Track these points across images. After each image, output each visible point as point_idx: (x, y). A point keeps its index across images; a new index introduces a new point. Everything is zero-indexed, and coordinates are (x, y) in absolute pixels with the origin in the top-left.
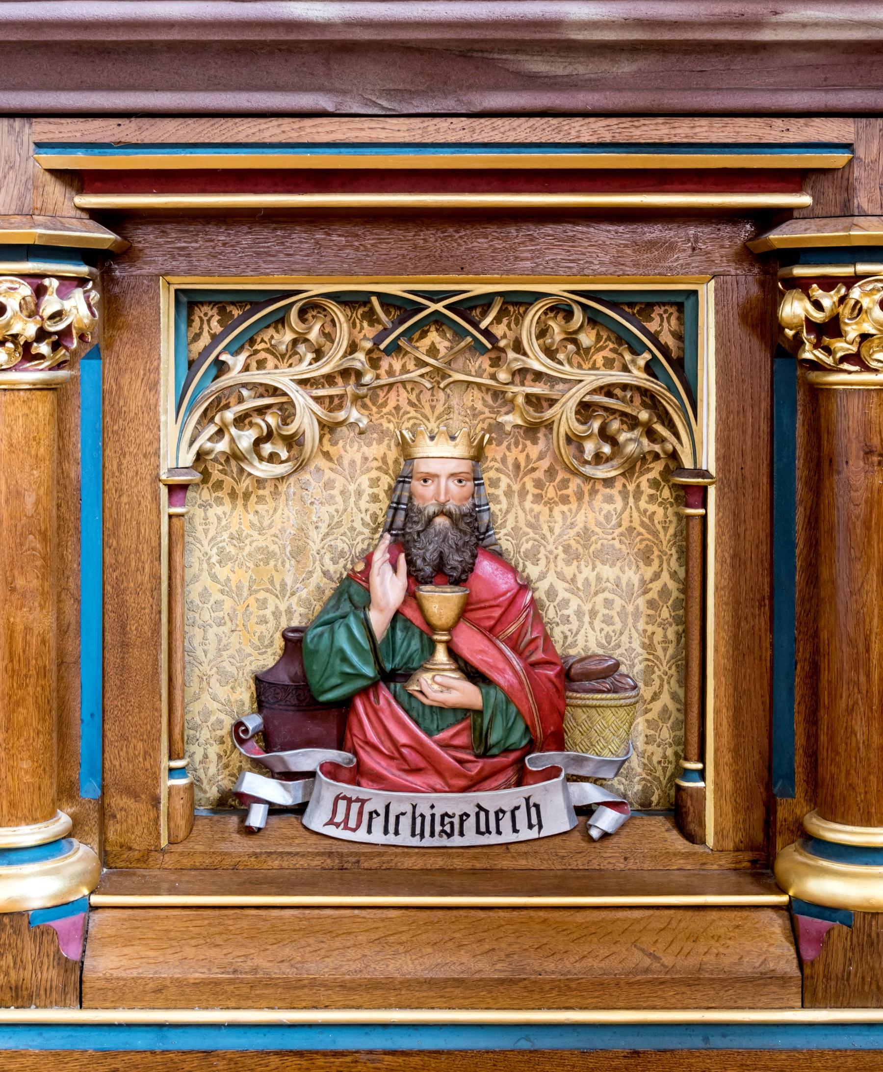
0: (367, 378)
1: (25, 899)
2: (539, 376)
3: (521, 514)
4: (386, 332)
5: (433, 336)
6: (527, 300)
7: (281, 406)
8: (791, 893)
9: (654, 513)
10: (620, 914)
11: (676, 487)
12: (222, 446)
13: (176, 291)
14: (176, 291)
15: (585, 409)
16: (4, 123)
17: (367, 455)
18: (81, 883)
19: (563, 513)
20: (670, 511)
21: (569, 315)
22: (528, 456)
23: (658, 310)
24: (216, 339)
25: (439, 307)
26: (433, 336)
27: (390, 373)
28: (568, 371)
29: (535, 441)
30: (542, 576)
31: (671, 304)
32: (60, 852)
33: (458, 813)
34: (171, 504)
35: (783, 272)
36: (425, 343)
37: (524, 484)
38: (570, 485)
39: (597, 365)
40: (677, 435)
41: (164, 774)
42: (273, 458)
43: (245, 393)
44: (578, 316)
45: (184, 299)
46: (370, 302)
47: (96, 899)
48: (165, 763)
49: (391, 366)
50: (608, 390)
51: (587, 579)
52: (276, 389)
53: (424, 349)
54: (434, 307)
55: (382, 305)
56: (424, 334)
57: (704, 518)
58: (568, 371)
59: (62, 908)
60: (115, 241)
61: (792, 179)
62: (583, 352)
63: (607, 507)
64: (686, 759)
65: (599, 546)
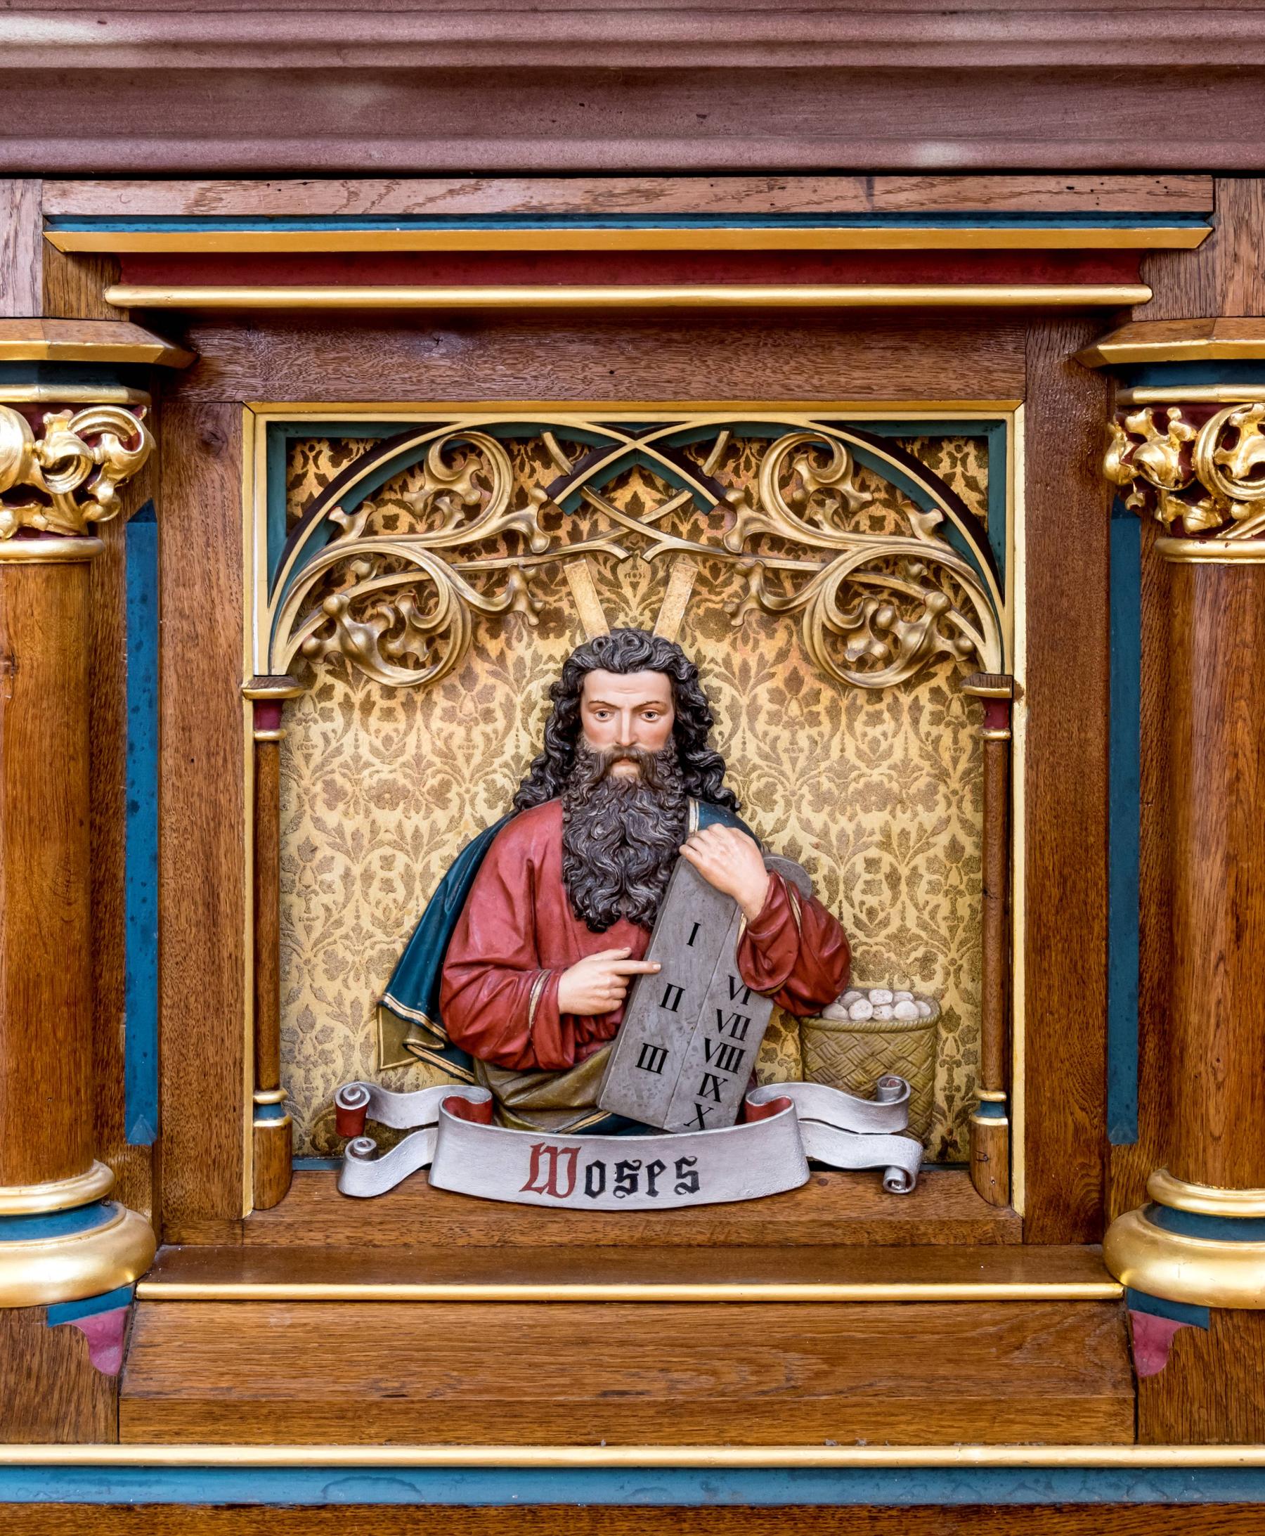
0: (540, 543)
1: (40, 1286)
2: (778, 543)
3: (425, 736)
4: (565, 480)
5: (637, 486)
6: (765, 436)
7: (420, 586)
8: (1124, 1279)
9: (777, 739)
10: (873, 1311)
11: (971, 699)
12: (332, 644)
13: (270, 426)
14: (270, 426)
15: (847, 593)
16: (7, 183)
17: (540, 651)
18: (128, 1265)
19: (485, 735)
20: (964, 735)
21: (824, 455)
22: (762, 656)
23: (948, 447)
24: (331, 488)
25: (640, 444)
26: (637, 486)
27: (575, 535)
28: (829, 535)
29: (771, 635)
30: (780, 826)
31: (968, 439)
32: (96, 1221)
33: (648, 1161)
34: (258, 725)
35: (1120, 395)
36: (622, 497)
37: (755, 697)
38: (822, 697)
39: (862, 528)
40: (977, 624)
41: (248, 1110)
42: (402, 660)
43: (363, 567)
44: (841, 460)
45: (282, 436)
46: (540, 438)
47: (143, 1288)
48: (250, 1097)
49: (575, 525)
50: (889, 563)
51: (417, 830)
52: (409, 563)
53: (620, 504)
54: (631, 444)
55: (562, 444)
56: (622, 481)
57: (1008, 744)
58: (829, 535)
59: (92, 1299)
60: (166, 351)
61: (1128, 265)
62: (845, 512)
63: (387, 727)
64: (984, 1088)
65: (860, 785)
